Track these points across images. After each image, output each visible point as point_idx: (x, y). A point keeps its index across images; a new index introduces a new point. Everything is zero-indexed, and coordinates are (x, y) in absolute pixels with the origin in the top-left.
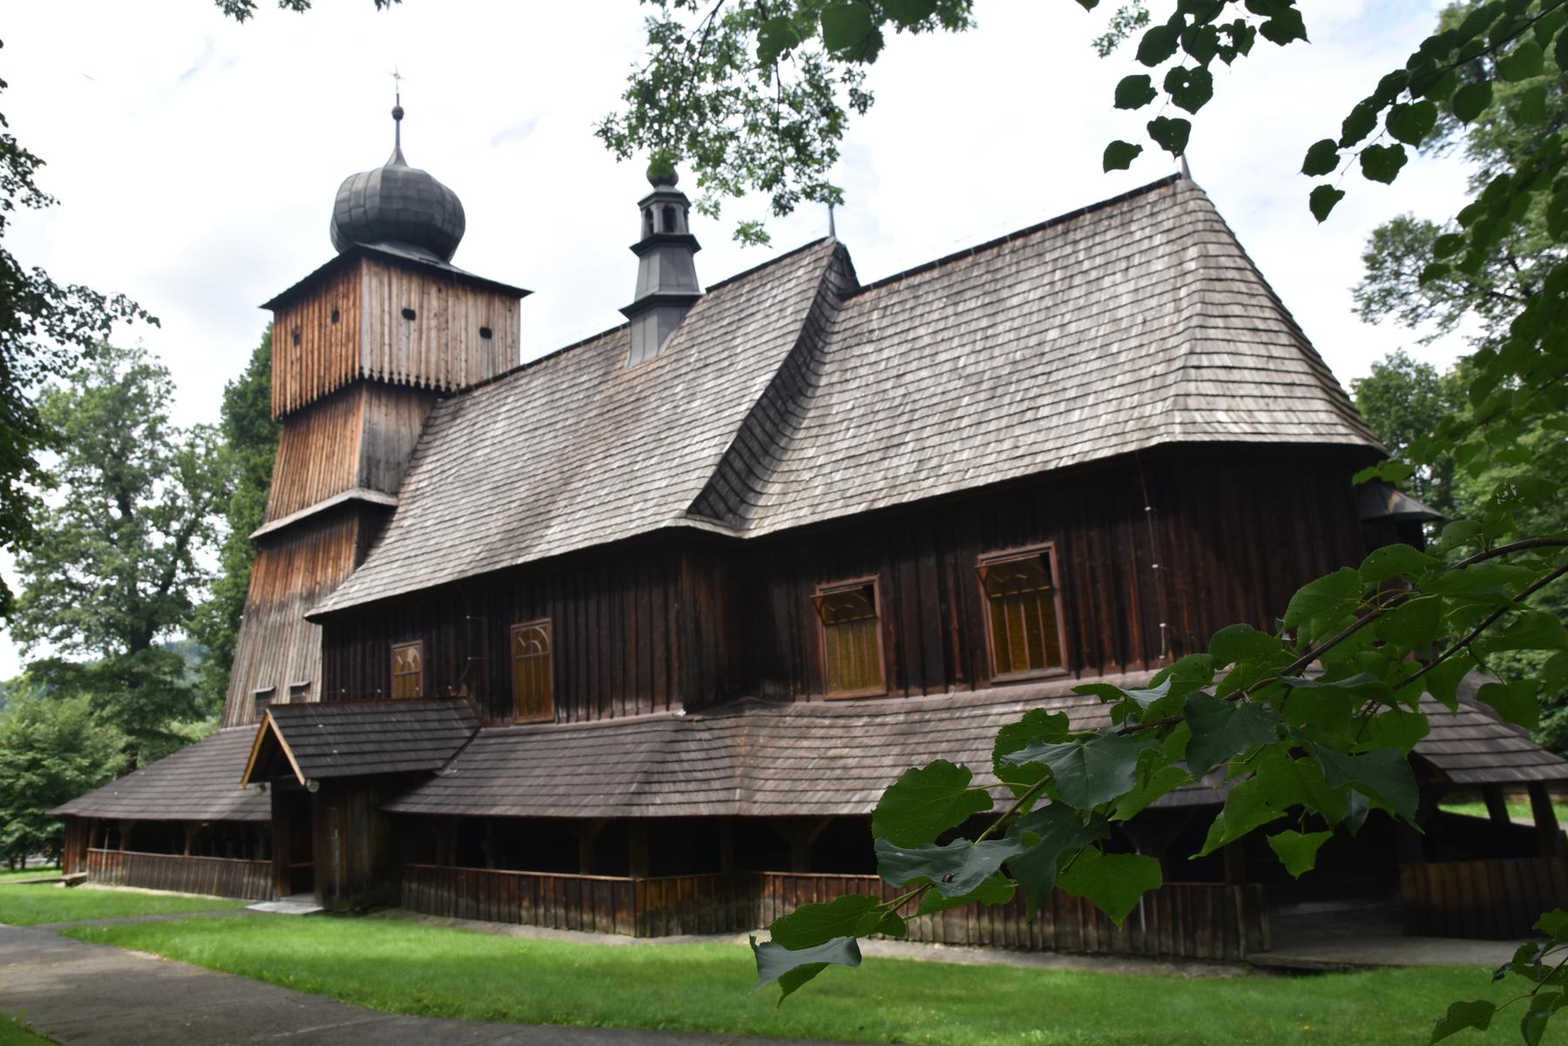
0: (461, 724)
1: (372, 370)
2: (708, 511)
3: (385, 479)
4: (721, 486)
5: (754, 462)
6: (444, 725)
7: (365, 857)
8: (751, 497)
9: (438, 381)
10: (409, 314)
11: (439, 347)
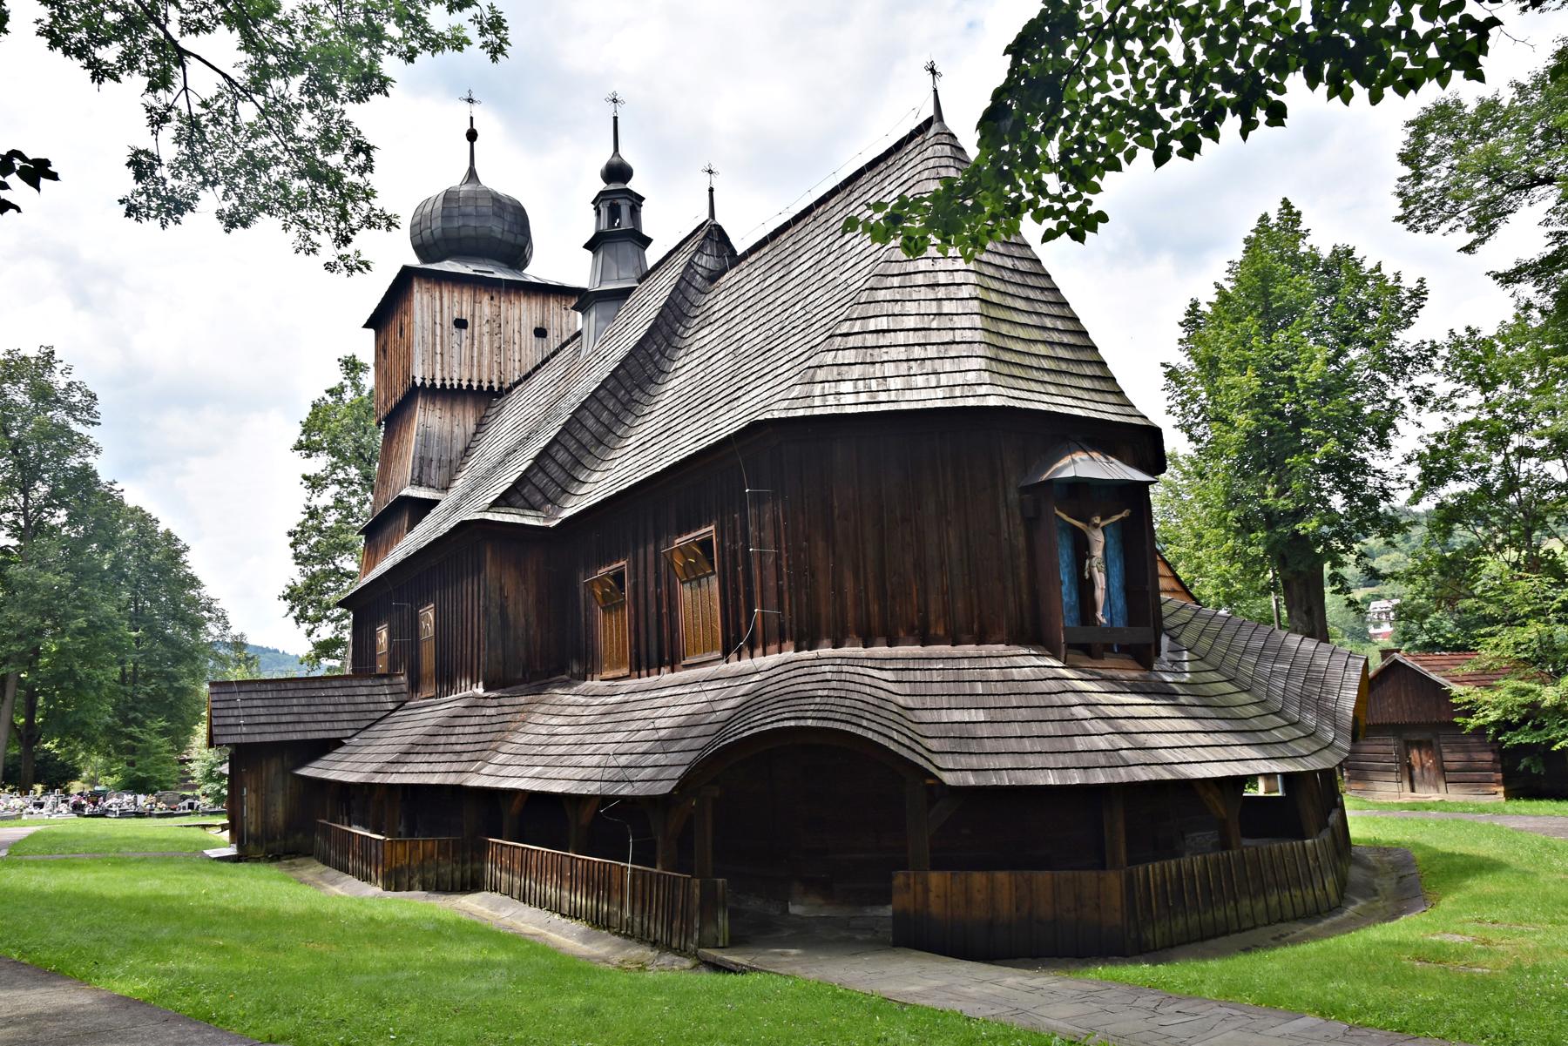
0: (389, 698)
1: (424, 379)
2: (522, 502)
3: (436, 475)
4: (540, 479)
5: (582, 452)
6: (371, 699)
7: (279, 813)
8: (574, 486)
9: (491, 382)
10: (461, 324)
11: (491, 352)
